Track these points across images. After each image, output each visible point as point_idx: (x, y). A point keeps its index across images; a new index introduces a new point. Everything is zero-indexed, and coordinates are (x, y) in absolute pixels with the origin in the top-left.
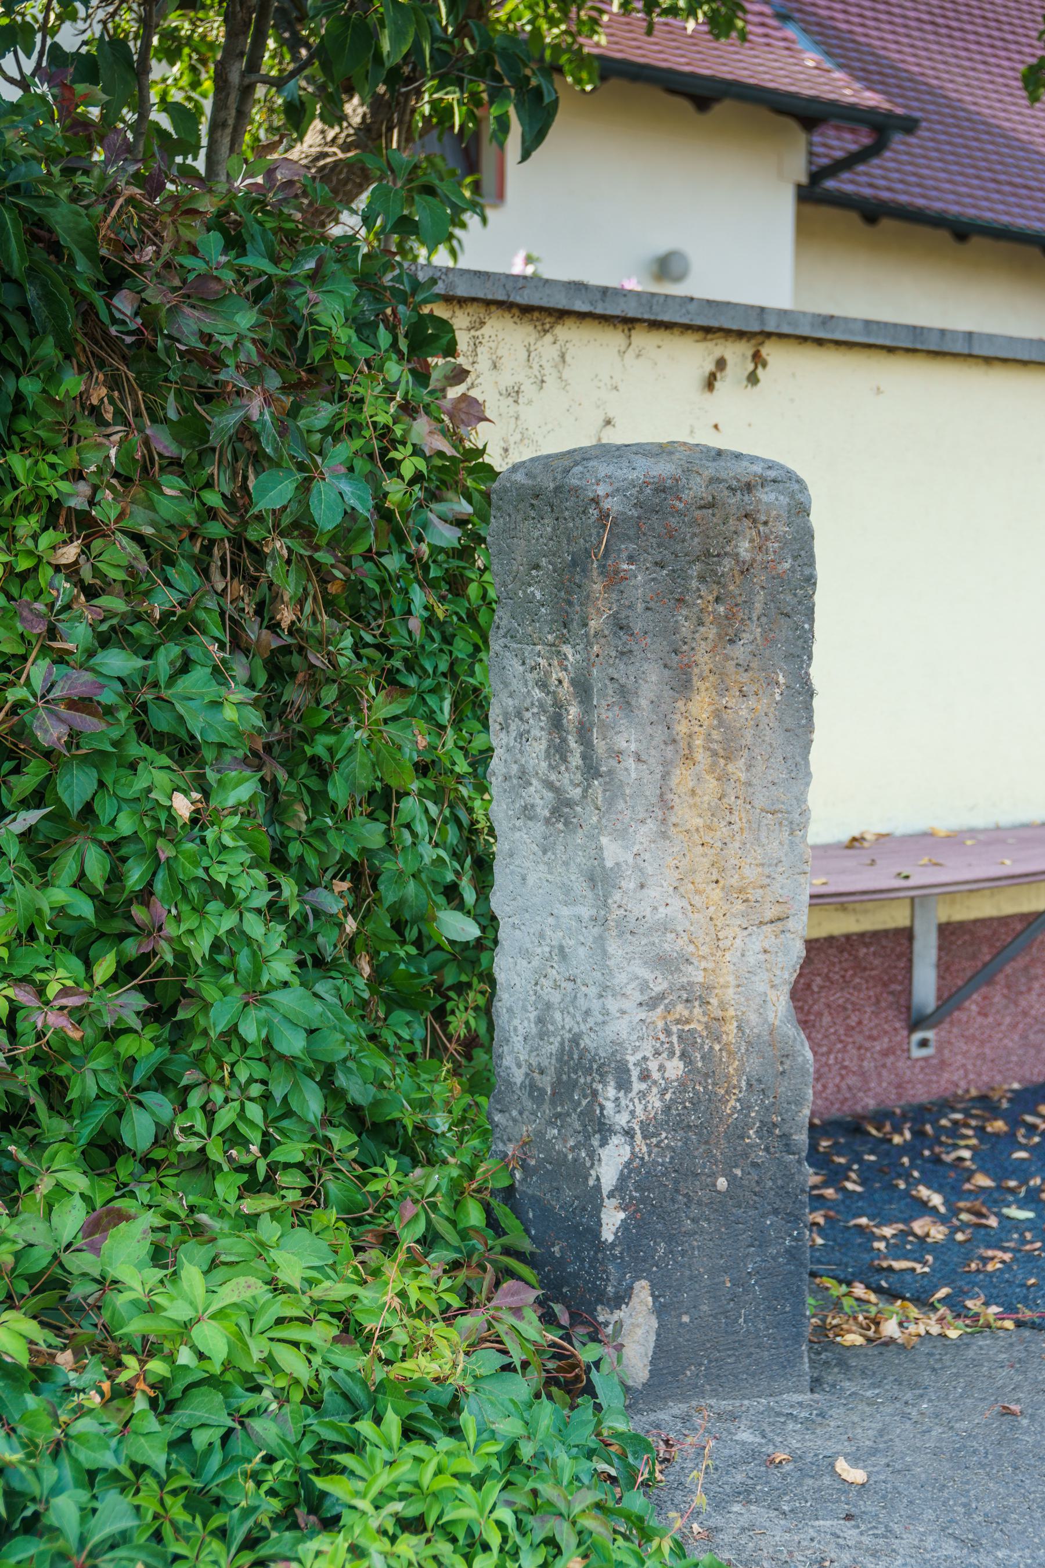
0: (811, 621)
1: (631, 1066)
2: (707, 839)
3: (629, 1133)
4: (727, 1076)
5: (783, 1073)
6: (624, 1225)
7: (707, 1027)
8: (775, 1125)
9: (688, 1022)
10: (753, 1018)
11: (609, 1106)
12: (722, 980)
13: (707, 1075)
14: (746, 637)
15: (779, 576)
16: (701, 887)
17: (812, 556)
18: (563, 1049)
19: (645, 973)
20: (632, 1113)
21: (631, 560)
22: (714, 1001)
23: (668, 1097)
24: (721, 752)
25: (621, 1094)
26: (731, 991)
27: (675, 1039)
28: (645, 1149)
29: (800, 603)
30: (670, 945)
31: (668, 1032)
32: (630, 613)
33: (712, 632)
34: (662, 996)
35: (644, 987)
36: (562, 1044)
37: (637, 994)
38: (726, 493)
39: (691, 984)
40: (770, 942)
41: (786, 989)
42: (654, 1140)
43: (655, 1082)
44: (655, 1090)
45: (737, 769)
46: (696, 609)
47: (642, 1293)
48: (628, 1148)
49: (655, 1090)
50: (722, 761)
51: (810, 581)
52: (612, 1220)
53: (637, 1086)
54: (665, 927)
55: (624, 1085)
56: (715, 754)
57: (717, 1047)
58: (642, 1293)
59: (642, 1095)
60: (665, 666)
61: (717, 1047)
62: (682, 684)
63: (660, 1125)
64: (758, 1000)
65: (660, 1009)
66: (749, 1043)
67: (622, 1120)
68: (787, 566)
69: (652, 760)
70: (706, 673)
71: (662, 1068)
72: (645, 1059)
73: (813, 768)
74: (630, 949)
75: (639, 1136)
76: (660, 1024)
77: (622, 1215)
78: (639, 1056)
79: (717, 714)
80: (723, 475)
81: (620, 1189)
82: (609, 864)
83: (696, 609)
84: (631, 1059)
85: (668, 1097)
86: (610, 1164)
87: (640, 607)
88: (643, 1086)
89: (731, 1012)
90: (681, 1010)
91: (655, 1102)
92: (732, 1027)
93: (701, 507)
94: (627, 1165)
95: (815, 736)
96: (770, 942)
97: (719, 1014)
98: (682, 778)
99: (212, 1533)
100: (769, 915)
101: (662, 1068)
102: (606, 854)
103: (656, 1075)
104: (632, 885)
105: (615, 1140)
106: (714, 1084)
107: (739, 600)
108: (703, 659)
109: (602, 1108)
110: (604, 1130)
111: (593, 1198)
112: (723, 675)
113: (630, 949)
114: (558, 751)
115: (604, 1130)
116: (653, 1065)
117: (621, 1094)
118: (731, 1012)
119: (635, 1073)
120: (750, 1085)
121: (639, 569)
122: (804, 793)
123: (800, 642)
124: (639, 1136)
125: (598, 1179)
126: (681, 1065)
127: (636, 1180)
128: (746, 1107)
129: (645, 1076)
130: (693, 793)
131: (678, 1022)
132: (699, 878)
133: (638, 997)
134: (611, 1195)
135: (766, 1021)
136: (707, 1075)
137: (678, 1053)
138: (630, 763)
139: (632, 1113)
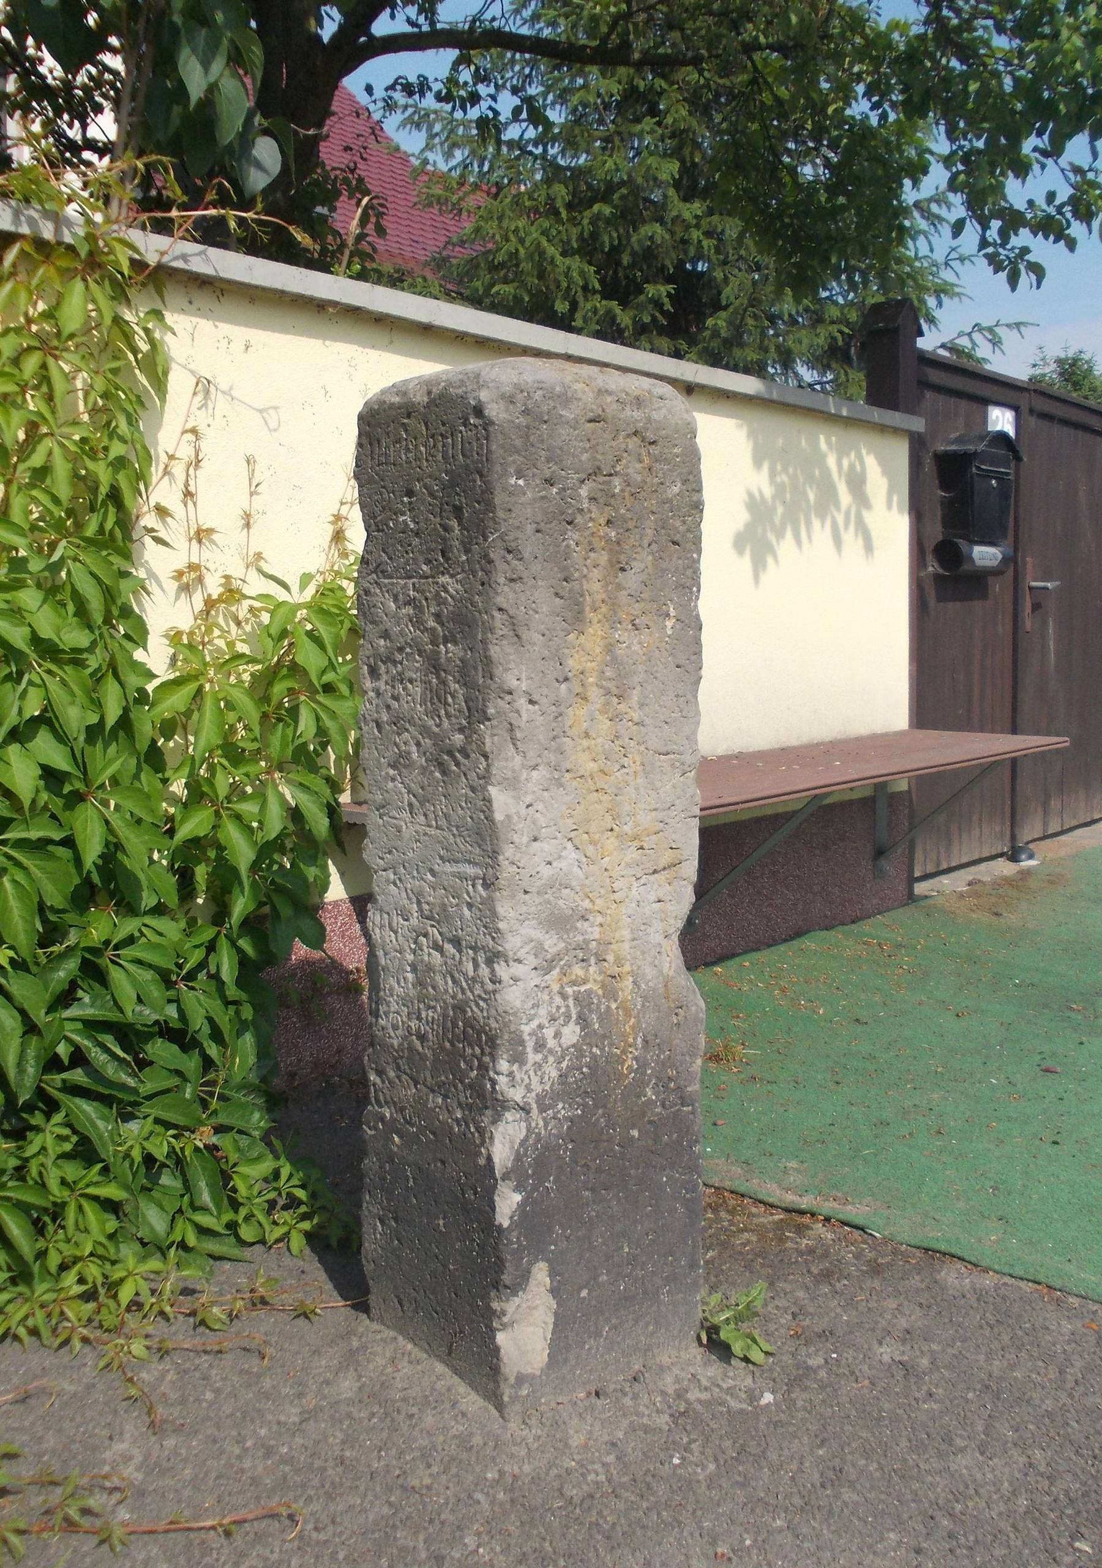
0: (699, 553)
1: (526, 1037)
2: (600, 784)
3: (525, 1109)
4: (624, 1036)
5: (678, 1024)
6: (521, 1206)
7: (603, 986)
8: (670, 1079)
9: (585, 982)
10: (649, 972)
11: (502, 1080)
12: (617, 935)
13: (604, 1037)
14: (637, 565)
15: (670, 501)
16: (597, 837)
17: (699, 482)
18: (445, 1016)
19: (538, 934)
20: (529, 1089)
21: (520, 475)
22: (610, 958)
23: (564, 1065)
24: (615, 691)
25: (515, 1067)
26: (626, 946)
27: (571, 1002)
28: (541, 1123)
29: (688, 530)
30: (567, 900)
31: (564, 996)
32: (518, 534)
33: (603, 558)
34: (557, 957)
35: (539, 949)
36: (445, 1009)
37: (531, 958)
38: (615, 406)
39: (587, 942)
40: (664, 891)
41: (675, 938)
42: (550, 1112)
43: (551, 1051)
44: (551, 1059)
45: (631, 709)
46: (587, 533)
47: (541, 1274)
48: (523, 1124)
49: (551, 1059)
50: (615, 700)
51: (698, 507)
52: (508, 1203)
53: (532, 1057)
54: (560, 884)
55: (518, 1058)
56: (608, 693)
57: (614, 1006)
58: (541, 1274)
59: (538, 1066)
60: (557, 594)
61: (614, 1006)
62: (575, 615)
63: (556, 1096)
64: (654, 952)
65: (556, 972)
66: (645, 998)
67: (517, 1095)
68: (676, 490)
69: (543, 701)
70: (599, 604)
71: (557, 1035)
72: (540, 1027)
73: (702, 707)
74: (524, 909)
75: (535, 1112)
76: (556, 987)
77: (517, 1198)
78: (534, 1024)
79: (609, 649)
80: (612, 387)
81: (517, 1174)
82: (499, 816)
83: (587, 533)
84: (526, 1029)
85: (564, 1065)
86: (505, 1142)
87: (530, 528)
88: (539, 1057)
89: (627, 968)
90: (578, 971)
91: (552, 1072)
92: (628, 982)
93: (590, 421)
94: (523, 1142)
95: (703, 672)
96: (664, 891)
97: (616, 970)
98: (578, 715)
99: (128, 1309)
100: (663, 862)
101: (557, 1035)
102: (495, 805)
103: (551, 1043)
104: (525, 839)
105: (509, 1116)
106: (611, 1045)
107: (631, 524)
108: (594, 587)
109: (494, 1083)
110: (498, 1105)
111: (484, 1179)
112: (614, 607)
113: (524, 909)
114: (437, 697)
115: (498, 1105)
116: (549, 1033)
117: (515, 1067)
118: (627, 968)
119: (530, 1044)
120: (646, 1041)
121: (527, 485)
122: (695, 732)
123: (689, 572)
124: (535, 1112)
125: (489, 1159)
126: (578, 1029)
127: (536, 1163)
128: (643, 1065)
129: (540, 1046)
130: (587, 735)
131: (574, 983)
132: (593, 827)
133: (532, 961)
134: (506, 1177)
135: (661, 972)
136: (604, 1037)
137: (574, 1017)
138: (522, 702)
139: (529, 1089)
